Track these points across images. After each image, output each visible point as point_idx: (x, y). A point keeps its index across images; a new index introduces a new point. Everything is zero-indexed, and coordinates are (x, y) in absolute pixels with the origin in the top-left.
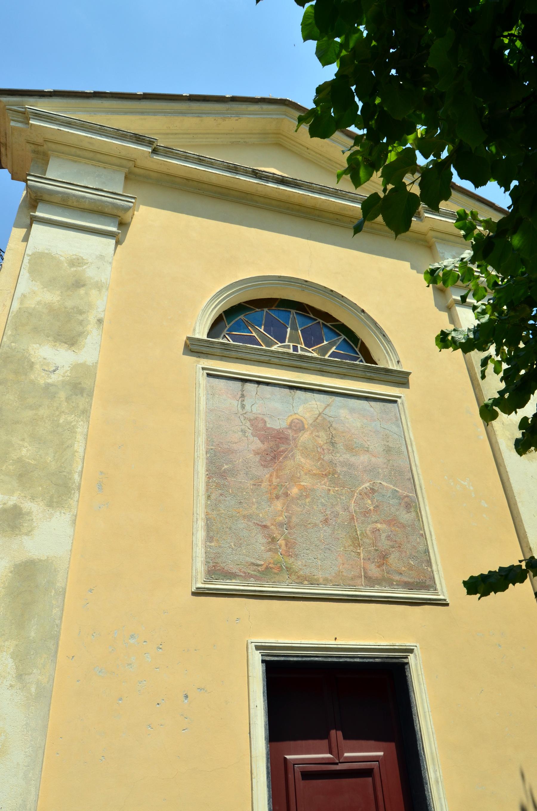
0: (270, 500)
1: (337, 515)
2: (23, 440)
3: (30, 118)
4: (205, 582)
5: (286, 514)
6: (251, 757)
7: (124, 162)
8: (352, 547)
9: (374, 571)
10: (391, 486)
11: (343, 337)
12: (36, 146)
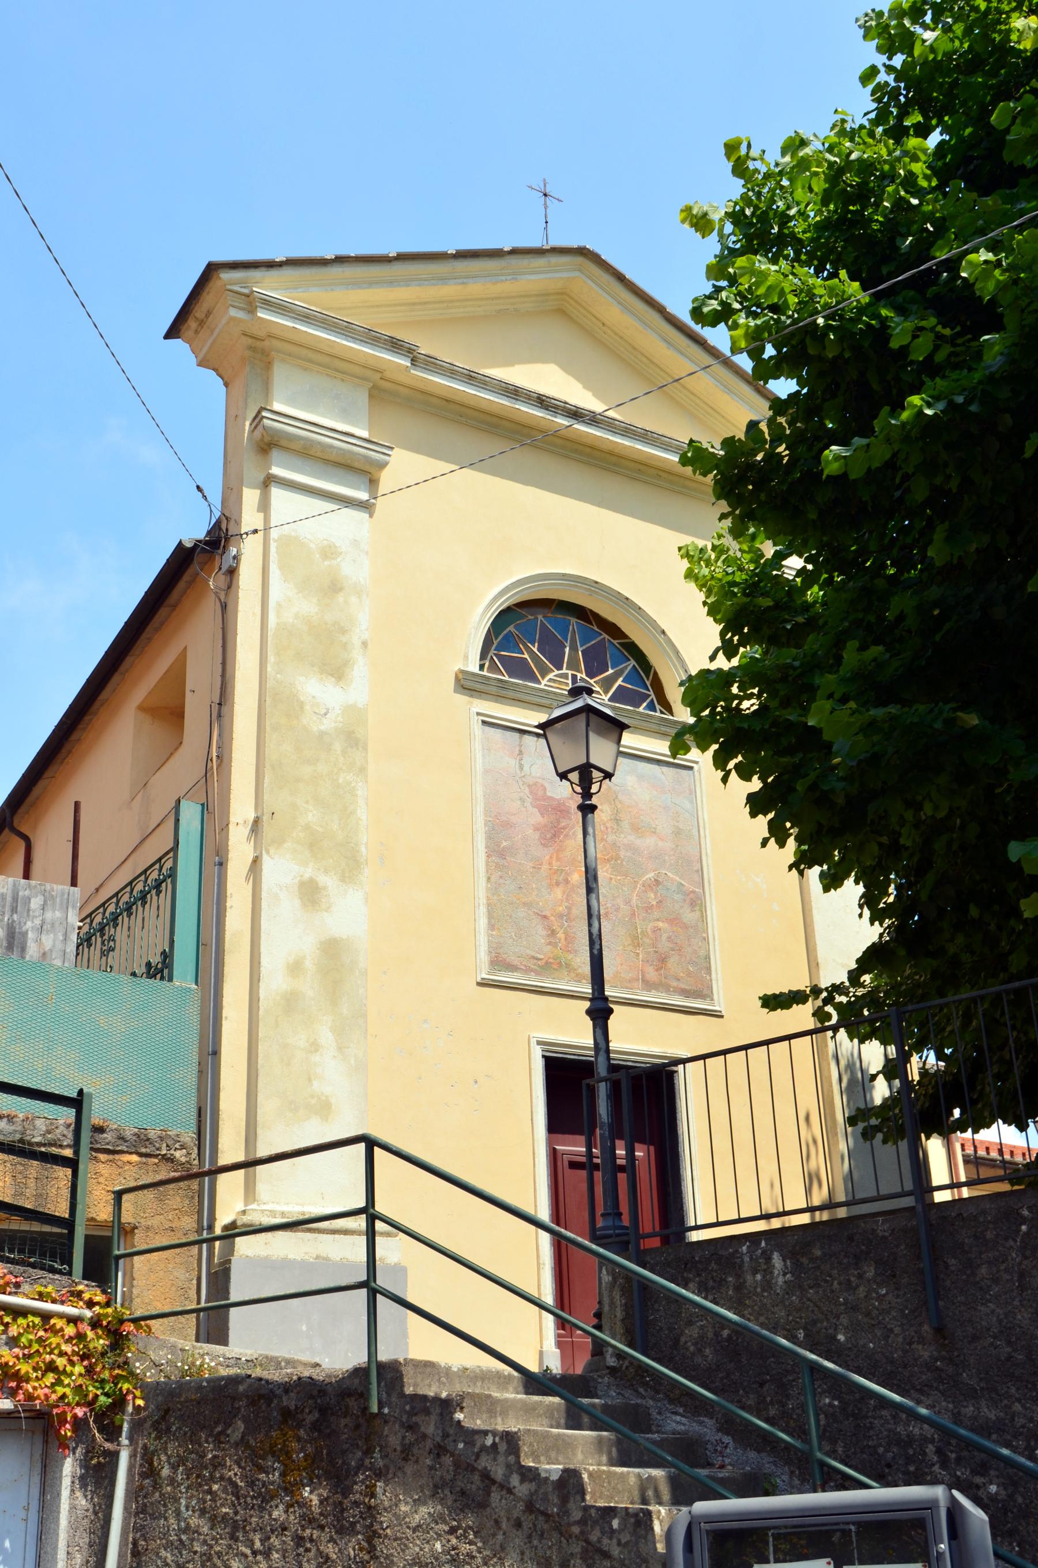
0: (551, 886)
1: (618, 909)
2: (307, 802)
3: (256, 307)
4: (489, 973)
5: (566, 904)
6: (533, 1140)
7: (369, 373)
8: (631, 947)
9: (652, 974)
10: (677, 878)
11: (633, 662)
12: (254, 340)
